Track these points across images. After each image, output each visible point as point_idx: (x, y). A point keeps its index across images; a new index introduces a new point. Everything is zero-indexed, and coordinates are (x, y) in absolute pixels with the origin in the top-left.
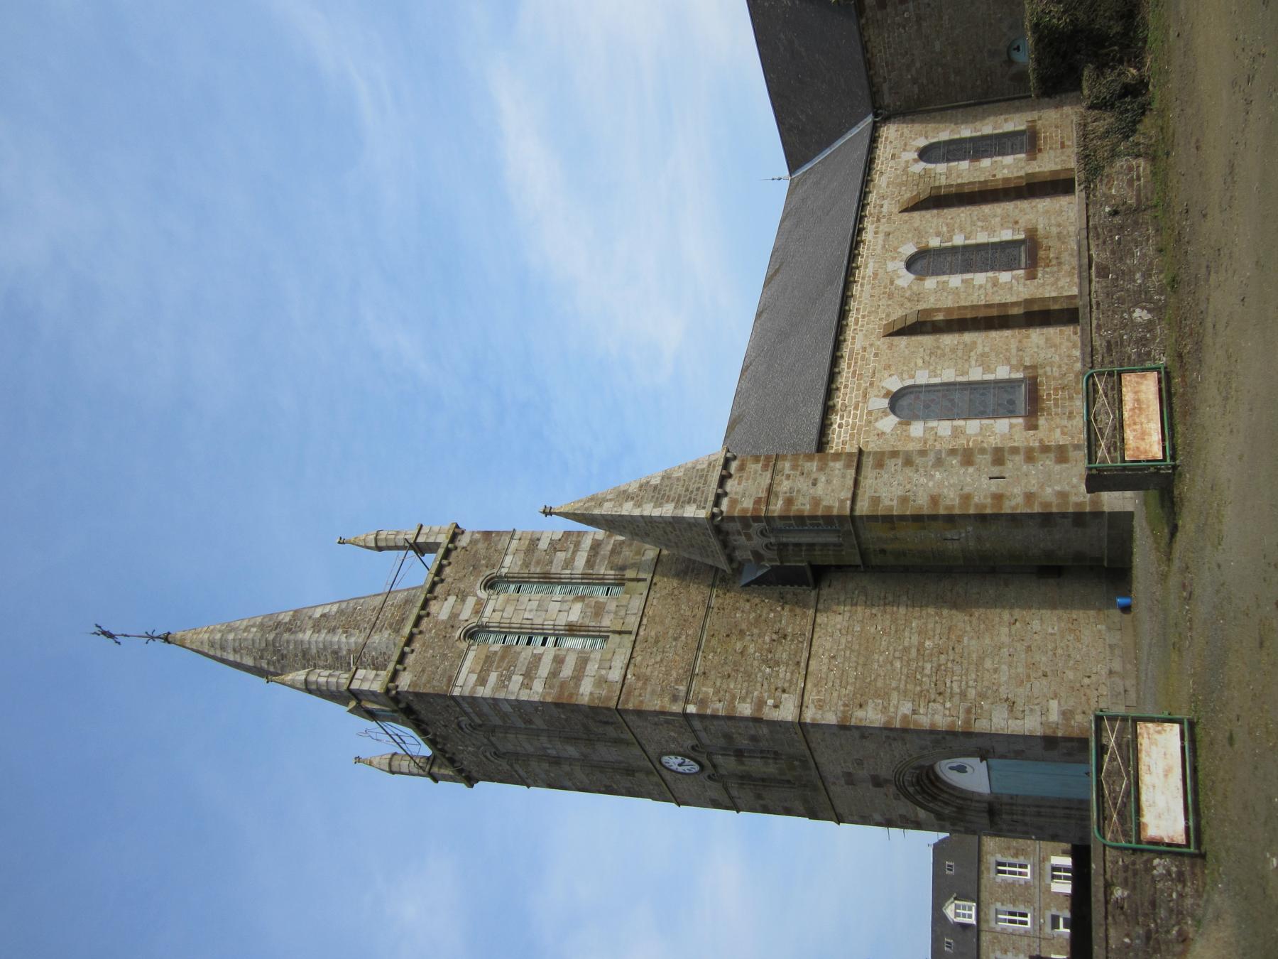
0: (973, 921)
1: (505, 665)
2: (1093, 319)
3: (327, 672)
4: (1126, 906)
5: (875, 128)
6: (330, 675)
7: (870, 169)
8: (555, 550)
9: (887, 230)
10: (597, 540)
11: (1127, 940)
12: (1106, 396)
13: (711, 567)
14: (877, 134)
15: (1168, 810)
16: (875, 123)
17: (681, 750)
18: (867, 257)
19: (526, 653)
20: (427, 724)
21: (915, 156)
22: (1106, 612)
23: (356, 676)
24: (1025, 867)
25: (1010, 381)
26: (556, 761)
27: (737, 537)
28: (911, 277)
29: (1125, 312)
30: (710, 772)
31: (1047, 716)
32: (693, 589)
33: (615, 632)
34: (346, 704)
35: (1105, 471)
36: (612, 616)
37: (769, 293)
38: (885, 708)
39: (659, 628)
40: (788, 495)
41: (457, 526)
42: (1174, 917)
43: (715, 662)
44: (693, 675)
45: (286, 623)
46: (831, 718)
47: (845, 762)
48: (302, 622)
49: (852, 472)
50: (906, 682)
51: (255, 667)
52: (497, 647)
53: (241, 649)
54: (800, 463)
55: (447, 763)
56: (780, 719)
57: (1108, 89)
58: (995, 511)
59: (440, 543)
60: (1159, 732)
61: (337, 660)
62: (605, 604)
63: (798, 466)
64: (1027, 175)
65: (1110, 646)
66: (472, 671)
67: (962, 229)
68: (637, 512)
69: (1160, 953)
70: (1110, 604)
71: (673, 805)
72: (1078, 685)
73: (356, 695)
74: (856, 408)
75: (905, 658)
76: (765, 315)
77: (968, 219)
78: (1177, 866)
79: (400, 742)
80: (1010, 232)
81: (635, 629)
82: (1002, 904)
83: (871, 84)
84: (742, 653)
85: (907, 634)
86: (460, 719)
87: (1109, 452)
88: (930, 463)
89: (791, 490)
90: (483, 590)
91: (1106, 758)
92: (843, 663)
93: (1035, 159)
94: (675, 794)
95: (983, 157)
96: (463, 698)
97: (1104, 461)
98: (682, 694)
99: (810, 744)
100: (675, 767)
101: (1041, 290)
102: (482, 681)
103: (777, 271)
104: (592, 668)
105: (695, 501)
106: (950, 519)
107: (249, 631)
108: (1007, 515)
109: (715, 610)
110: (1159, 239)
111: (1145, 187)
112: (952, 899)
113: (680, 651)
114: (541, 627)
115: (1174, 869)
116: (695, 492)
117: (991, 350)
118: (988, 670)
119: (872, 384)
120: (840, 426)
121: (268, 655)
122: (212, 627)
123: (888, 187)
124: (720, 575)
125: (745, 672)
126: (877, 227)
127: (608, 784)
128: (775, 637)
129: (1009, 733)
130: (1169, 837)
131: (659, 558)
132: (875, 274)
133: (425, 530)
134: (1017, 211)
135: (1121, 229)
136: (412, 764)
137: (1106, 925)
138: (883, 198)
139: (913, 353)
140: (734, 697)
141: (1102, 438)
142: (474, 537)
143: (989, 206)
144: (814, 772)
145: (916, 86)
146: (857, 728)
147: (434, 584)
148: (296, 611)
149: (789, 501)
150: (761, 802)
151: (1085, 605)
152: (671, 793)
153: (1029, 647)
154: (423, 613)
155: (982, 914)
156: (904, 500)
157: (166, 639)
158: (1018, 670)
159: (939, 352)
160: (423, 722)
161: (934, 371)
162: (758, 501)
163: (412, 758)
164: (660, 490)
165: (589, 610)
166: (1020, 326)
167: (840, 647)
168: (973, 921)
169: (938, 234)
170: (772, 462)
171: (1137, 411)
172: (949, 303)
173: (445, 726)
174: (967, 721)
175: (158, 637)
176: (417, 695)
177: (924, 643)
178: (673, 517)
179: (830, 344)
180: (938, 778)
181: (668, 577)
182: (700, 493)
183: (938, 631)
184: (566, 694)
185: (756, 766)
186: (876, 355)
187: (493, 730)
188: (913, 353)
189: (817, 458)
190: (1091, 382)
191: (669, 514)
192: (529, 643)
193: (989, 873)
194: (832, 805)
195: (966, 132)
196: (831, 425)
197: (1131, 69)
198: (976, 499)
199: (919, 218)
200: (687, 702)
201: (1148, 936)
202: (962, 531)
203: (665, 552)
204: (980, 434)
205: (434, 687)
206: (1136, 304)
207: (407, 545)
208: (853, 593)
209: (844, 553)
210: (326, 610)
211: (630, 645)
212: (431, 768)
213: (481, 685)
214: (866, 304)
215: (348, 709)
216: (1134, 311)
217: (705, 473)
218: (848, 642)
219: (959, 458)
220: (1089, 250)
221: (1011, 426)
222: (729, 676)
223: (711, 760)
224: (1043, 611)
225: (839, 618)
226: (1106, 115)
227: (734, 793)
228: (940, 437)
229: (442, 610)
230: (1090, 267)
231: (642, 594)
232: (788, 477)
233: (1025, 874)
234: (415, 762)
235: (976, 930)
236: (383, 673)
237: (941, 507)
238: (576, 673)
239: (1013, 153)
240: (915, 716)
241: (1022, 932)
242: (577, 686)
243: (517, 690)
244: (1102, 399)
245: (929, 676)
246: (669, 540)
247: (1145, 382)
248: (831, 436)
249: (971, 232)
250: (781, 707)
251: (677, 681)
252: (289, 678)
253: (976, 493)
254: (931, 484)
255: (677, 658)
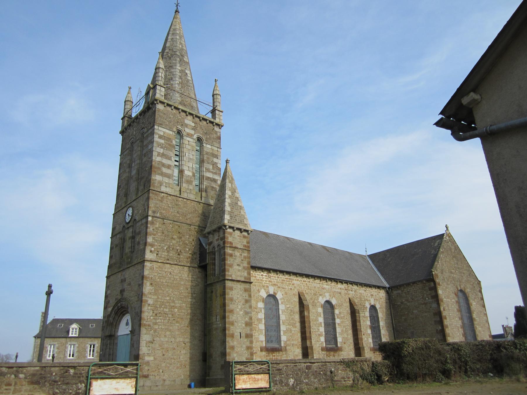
0: (70, 335)
1: (167, 146)
2: (290, 364)
3: (163, 76)
4: (67, 374)
5: (384, 288)
6: (162, 77)
7: (367, 286)
8: (213, 165)
9: (342, 293)
10: (217, 181)
11: (54, 374)
12: (260, 368)
13: (206, 226)
14: (381, 289)
15: (102, 389)
16: (386, 288)
17: (134, 215)
18: (331, 285)
19: (172, 154)
20: (143, 116)
21: (372, 304)
22: (189, 378)
23: (162, 88)
24: (93, 356)
25: (280, 341)
26: (130, 166)
27: (217, 235)
28: (323, 302)
29: (293, 376)
30: (126, 227)
31: (147, 356)
32: (198, 219)
33: (180, 188)
34: (152, 83)
35: (232, 368)
36: (187, 187)
37: (319, 248)
38: (151, 293)
39: (182, 206)
40: (234, 255)
41: (222, 126)
42: (63, 391)
43: (169, 228)
44: (163, 219)
45: (183, 59)
46: (146, 273)
47: (130, 279)
48: (184, 65)
49: (243, 280)
50: (161, 302)
51: (166, 47)
52: (174, 142)
53: (173, 41)
54: (247, 260)
55: (129, 123)
56: (146, 253)
57: (380, 369)
58: (227, 335)
59: (216, 120)
60: (132, 386)
61: (169, 80)
62: (192, 184)
63: (245, 259)
64: (364, 348)
65: (175, 380)
66: (164, 133)
67: (342, 322)
68: (227, 196)
69: (50, 386)
70: (192, 380)
71: (113, 212)
72: (159, 368)
73: (155, 88)
74: (269, 281)
75: (170, 301)
76: (310, 246)
77: (346, 325)
78: (81, 392)
79: (137, 105)
80: (341, 341)
81: (181, 196)
82: (77, 347)
83: (401, 286)
84: (172, 238)
85: (180, 302)
86: (146, 129)
87: (238, 369)
88: (246, 310)
89: (235, 256)
90: (197, 137)
91: (123, 367)
92: (168, 277)
93: (371, 350)
94: (117, 213)
95: (371, 330)
96: (154, 130)
97: (235, 367)
98: (156, 215)
99: (136, 265)
100: (128, 213)
101: (317, 353)
102: (160, 137)
103: (328, 251)
104: (166, 180)
105: (231, 219)
106: (224, 317)
107: (180, 44)
108: (226, 339)
109: (189, 228)
110: (321, 388)
111: (341, 383)
112: (79, 327)
113: (173, 214)
114: (182, 159)
115: (80, 391)
116: (235, 219)
117: (293, 334)
118: (165, 333)
119: (279, 287)
120: (262, 275)
121: (170, 52)
122: (181, 29)
123: (359, 293)
124: (203, 229)
125: (165, 239)
126: (343, 289)
127: (122, 186)
128: (179, 251)
129: (141, 341)
130: (92, 389)
131: (210, 205)
132: (324, 288)
133: (221, 113)
134: (349, 343)
135: (325, 375)
136: (129, 110)
137: (60, 367)
138: (355, 291)
139: (292, 303)
140: (155, 235)
141: (244, 367)
142: (218, 133)
143: (351, 333)
144: (126, 267)
145: (400, 303)
146: (143, 283)
147: (199, 117)
148: (188, 63)
149: (231, 255)
150: (115, 247)
151: (191, 371)
152: (118, 211)
153: (175, 349)
154: (188, 113)
155: (73, 339)
156: (232, 300)
157: (177, 11)
158: (165, 345)
159: (292, 313)
160: (145, 113)
161: (284, 312)
162: (231, 243)
163: (131, 109)
164: (236, 205)
165: (189, 178)
166: (302, 345)
167: (175, 276)
168: (70, 335)
169: (340, 313)
170: (247, 249)
171: (254, 379)
172: (312, 317)
173: (143, 123)
174: (145, 325)
175: (177, 8)
176: (155, 111)
177: (176, 308)
178: (225, 210)
179: (295, 271)
180: (124, 315)
181: (202, 209)
182: (235, 221)
183: (181, 314)
184: (156, 170)
185: (128, 244)
186: (291, 289)
187: (142, 142)
188: (292, 303)
189: (248, 266)
190: (266, 363)
191: (226, 209)
192: (176, 155)
193: (90, 341)
194: (113, 274)
195: (382, 324)
196: (263, 272)
197: (388, 378)
198: (232, 327)
199: (347, 305)
200: (153, 217)
201: (55, 381)
202: (220, 322)
203: (212, 207)
204: (259, 329)
205: (158, 118)
206: (296, 380)
207: (215, 106)
208: (196, 281)
209: (211, 277)
210: (189, 75)
211: (175, 194)
212: (127, 117)
213: (159, 136)
214: (312, 285)
215: (150, 84)
216: (293, 379)
217: (242, 222)
218: (177, 279)
219: (248, 321)
220: (317, 362)
221: (262, 341)
222: (163, 233)
223: (130, 227)
224: (189, 355)
225: (186, 276)
226: (370, 370)
227: (118, 236)
228: (258, 314)
229: (189, 121)
230: (310, 363)
231: (196, 199)
232: (241, 255)
233: (90, 356)
234: (129, 111)
235: (67, 336)
236: (163, 98)
237: (229, 314)
238: (164, 174)
239: (373, 342)
240: (147, 305)
241: (66, 355)
242: (159, 174)
243: (157, 151)
244: (259, 367)
245: (163, 311)
246: (216, 209)
247: (265, 383)
248: (258, 272)
249: (341, 326)
250: (151, 253)
251: (161, 213)
252: (161, 61)
253: (234, 327)
254: (238, 310)
255: (170, 213)
